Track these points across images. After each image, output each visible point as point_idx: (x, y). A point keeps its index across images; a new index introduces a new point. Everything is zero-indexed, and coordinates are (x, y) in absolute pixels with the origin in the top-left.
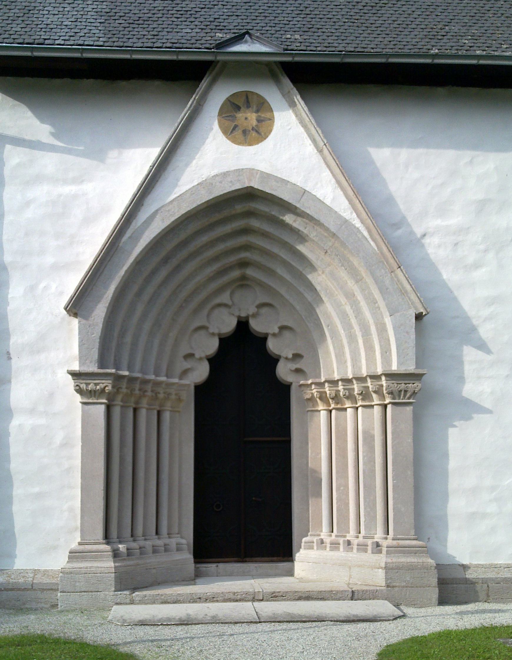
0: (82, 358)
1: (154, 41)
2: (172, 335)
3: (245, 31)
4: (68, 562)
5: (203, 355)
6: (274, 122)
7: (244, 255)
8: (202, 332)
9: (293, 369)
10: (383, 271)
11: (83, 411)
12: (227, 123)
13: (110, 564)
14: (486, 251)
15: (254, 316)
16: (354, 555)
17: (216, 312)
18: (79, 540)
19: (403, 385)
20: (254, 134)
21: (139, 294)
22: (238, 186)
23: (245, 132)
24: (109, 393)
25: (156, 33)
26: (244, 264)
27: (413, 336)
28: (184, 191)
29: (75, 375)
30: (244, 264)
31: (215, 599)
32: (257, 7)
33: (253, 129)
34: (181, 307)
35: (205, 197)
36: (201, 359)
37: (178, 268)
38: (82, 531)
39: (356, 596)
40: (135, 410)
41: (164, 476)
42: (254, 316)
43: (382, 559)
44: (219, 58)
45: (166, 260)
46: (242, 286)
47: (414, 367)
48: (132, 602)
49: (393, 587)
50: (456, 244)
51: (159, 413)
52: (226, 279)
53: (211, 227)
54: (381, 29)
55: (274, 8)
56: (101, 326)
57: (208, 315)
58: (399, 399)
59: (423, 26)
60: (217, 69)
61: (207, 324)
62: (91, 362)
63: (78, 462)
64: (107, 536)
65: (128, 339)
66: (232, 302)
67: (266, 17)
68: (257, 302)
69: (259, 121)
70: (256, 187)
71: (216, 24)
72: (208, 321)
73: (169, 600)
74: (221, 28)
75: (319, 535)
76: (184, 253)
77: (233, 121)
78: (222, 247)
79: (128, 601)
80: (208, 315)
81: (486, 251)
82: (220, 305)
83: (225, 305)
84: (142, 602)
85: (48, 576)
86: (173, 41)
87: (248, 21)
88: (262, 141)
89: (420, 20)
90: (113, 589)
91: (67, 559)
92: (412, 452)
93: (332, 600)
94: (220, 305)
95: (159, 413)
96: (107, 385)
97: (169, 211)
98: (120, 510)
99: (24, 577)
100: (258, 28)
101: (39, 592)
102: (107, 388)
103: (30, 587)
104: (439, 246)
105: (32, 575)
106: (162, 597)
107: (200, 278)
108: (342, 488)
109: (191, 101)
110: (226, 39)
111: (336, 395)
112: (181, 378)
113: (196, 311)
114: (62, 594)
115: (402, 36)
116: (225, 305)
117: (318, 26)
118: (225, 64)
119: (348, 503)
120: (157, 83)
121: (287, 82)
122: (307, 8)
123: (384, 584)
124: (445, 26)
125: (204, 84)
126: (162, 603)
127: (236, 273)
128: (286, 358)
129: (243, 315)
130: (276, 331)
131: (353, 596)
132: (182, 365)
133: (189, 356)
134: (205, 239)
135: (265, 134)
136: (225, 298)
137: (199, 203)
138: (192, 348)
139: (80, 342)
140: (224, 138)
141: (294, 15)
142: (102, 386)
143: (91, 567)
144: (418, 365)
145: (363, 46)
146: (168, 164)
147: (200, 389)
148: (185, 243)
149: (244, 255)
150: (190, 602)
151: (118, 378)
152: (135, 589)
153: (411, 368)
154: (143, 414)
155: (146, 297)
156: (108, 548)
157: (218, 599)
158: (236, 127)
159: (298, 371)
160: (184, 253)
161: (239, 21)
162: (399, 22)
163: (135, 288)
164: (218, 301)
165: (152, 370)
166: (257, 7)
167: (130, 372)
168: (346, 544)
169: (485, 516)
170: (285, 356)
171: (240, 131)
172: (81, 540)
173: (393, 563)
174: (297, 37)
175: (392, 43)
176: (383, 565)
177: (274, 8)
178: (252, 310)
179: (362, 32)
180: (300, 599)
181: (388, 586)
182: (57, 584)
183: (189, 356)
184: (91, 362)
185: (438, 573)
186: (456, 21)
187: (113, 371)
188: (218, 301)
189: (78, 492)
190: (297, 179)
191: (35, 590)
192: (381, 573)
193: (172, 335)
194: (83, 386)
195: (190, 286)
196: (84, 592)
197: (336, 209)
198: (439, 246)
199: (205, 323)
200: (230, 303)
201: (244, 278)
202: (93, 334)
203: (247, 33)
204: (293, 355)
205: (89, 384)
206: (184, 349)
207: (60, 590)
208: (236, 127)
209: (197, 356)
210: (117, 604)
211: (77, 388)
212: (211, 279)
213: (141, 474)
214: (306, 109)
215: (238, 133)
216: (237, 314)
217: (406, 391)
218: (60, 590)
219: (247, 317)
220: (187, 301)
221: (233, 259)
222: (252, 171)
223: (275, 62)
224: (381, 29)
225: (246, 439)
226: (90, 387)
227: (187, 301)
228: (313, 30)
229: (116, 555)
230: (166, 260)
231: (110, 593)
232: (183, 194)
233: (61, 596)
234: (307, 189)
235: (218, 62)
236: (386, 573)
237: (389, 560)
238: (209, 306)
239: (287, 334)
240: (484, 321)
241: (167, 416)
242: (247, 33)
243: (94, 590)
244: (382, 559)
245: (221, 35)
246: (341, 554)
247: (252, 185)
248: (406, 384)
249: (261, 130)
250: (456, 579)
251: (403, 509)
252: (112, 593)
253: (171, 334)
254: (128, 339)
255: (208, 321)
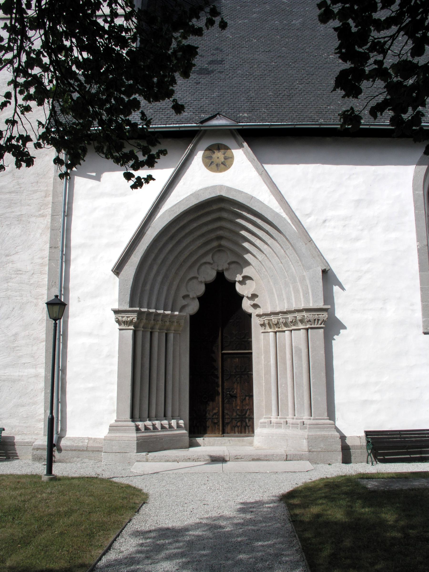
0: (120, 300)
1: (167, 121)
2: (176, 283)
3: (217, 113)
4: (109, 433)
5: (195, 296)
6: (233, 159)
7: (220, 233)
8: (195, 281)
9: (252, 304)
10: (300, 243)
11: (120, 334)
12: (207, 160)
13: (134, 435)
14: (362, 230)
15: (227, 269)
16: (290, 432)
17: (203, 267)
18: (115, 418)
19: (316, 315)
20: (222, 166)
21: (155, 259)
22: (213, 195)
23: (217, 165)
24: (135, 323)
25: (169, 116)
26: (220, 238)
27: (321, 284)
28: (182, 199)
29: (116, 312)
30: (220, 238)
31: (199, 460)
32: (224, 99)
33: (222, 163)
34: (181, 265)
35: (194, 202)
36: (193, 298)
37: (179, 242)
38: (117, 413)
39: (288, 458)
40: (151, 333)
41: (170, 378)
42: (227, 269)
43: (306, 433)
44: (202, 128)
45: (172, 238)
46: (219, 251)
47: (323, 304)
48: (147, 461)
49: (313, 452)
50: (345, 226)
51: (167, 335)
52: (209, 247)
53: (199, 217)
54: (292, 109)
55: (234, 99)
56: (132, 280)
57: (198, 270)
58: (314, 325)
59: (315, 107)
60: (201, 133)
61: (198, 276)
62: (125, 303)
63: (116, 368)
64: (133, 418)
65: (148, 287)
66: (213, 261)
67: (229, 104)
68: (229, 261)
69: (225, 158)
70: (224, 195)
71: (201, 109)
72: (198, 274)
73: (170, 460)
74: (204, 111)
75: (270, 418)
76: (183, 233)
77: (210, 159)
78: (205, 229)
79: (144, 459)
80: (198, 270)
81: (362, 230)
82: (205, 263)
83: (209, 263)
84: (153, 460)
85: (97, 442)
86: (178, 120)
87: (219, 107)
88: (227, 169)
89: (314, 103)
90: (136, 451)
91: (108, 431)
92: (324, 360)
93: (274, 461)
94: (205, 263)
95: (167, 335)
96: (134, 317)
97: (173, 210)
98: (141, 400)
99: (82, 442)
100: (224, 111)
101: (91, 452)
102: (134, 320)
103: (86, 449)
104: (335, 227)
105: (87, 441)
106: (166, 458)
107: (193, 247)
108: (283, 385)
109: (187, 150)
110: (206, 118)
111: (278, 322)
112: (180, 311)
113: (191, 267)
114: (105, 454)
115: (303, 113)
116: (209, 263)
117: (257, 108)
118: (205, 131)
119: (288, 396)
120: (169, 140)
121: (240, 138)
122: (251, 98)
123: (307, 450)
124: (328, 106)
125: (194, 141)
126: (166, 461)
127: (215, 244)
128: (247, 297)
129: (220, 269)
130: (241, 279)
131: (287, 459)
132: (181, 302)
133: (185, 297)
134: (195, 225)
135: (229, 166)
136: (208, 258)
137: (191, 205)
138: (188, 291)
139: (119, 291)
140: (206, 169)
141: (244, 103)
142: (131, 318)
143: (122, 437)
144: (325, 303)
145: (281, 119)
146: (174, 184)
147: (193, 318)
148: (183, 228)
149: (220, 233)
150: (183, 461)
151: (140, 314)
152: (149, 452)
153: (320, 304)
154: (156, 335)
155: (159, 261)
156: (133, 424)
157: (201, 460)
158: (212, 162)
159: (255, 306)
160: (183, 233)
161: (214, 107)
162: (302, 105)
163: (153, 256)
164: (204, 260)
165: (162, 306)
166: (224, 99)
167: (148, 309)
168: (285, 423)
169: (372, 402)
170: (246, 296)
171: (215, 165)
172: (117, 418)
173: (312, 435)
174: (246, 115)
175: (298, 117)
176: (306, 437)
177: (234, 99)
178: (226, 266)
179: (281, 111)
180: (253, 460)
181: (309, 451)
182: (102, 447)
183: (185, 297)
184: (125, 303)
185: (342, 442)
186: (334, 103)
187: (138, 309)
188: (204, 260)
189: (115, 387)
190: (248, 190)
191: (89, 451)
192: (305, 442)
193: (176, 283)
194: (120, 318)
195: (187, 253)
196: (118, 453)
197: (271, 207)
198: (335, 227)
199: (196, 275)
200: (212, 262)
201: (220, 246)
202: (127, 285)
203: (218, 114)
204: (252, 295)
205: (124, 317)
206: (183, 292)
207: (103, 451)
208: (212, 162)
209: (191, 296)
210: (137, 461)
211: (117, 319)
212: (200, 247)
213: (154, 375)
214: (251, 152)
215: (214, 166)
216: (216, 268)
217: (318, 320)
218: (103, 451)
219: (223, 271)
220: (185, 261)
221: (213, 235)
222: (221, 187)
223: (234, 129)
224: (292, 109)
225: (223, 352)
226: (124, 319)
227: (185, 261)
228: (255, 110)
229: (138, 429)
230: (172, 238)
231: (133, 454)
232: (182, 200)
233: (104, 455)
234: (254, 196)
235: (201, 130)
236: (308, 442)
237: (310, 434)
238: (199, 264)
239: (248, 282)
240: (365, 273)
241: (171, 336)
242: (218, 114)
243: (124, 451)
244: (306, 433)
245: (204, 116)
246: (282, 431)
247: (222, 194)
248: (318, 315)
249: (227, 164)
250: (354, 446)
251: (319, 399)
252: (135, 454)
253: (175, 283)
254: (148, 287)
255: (198, 274)
